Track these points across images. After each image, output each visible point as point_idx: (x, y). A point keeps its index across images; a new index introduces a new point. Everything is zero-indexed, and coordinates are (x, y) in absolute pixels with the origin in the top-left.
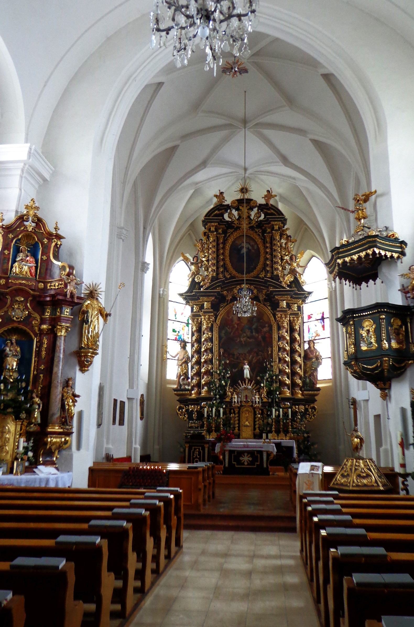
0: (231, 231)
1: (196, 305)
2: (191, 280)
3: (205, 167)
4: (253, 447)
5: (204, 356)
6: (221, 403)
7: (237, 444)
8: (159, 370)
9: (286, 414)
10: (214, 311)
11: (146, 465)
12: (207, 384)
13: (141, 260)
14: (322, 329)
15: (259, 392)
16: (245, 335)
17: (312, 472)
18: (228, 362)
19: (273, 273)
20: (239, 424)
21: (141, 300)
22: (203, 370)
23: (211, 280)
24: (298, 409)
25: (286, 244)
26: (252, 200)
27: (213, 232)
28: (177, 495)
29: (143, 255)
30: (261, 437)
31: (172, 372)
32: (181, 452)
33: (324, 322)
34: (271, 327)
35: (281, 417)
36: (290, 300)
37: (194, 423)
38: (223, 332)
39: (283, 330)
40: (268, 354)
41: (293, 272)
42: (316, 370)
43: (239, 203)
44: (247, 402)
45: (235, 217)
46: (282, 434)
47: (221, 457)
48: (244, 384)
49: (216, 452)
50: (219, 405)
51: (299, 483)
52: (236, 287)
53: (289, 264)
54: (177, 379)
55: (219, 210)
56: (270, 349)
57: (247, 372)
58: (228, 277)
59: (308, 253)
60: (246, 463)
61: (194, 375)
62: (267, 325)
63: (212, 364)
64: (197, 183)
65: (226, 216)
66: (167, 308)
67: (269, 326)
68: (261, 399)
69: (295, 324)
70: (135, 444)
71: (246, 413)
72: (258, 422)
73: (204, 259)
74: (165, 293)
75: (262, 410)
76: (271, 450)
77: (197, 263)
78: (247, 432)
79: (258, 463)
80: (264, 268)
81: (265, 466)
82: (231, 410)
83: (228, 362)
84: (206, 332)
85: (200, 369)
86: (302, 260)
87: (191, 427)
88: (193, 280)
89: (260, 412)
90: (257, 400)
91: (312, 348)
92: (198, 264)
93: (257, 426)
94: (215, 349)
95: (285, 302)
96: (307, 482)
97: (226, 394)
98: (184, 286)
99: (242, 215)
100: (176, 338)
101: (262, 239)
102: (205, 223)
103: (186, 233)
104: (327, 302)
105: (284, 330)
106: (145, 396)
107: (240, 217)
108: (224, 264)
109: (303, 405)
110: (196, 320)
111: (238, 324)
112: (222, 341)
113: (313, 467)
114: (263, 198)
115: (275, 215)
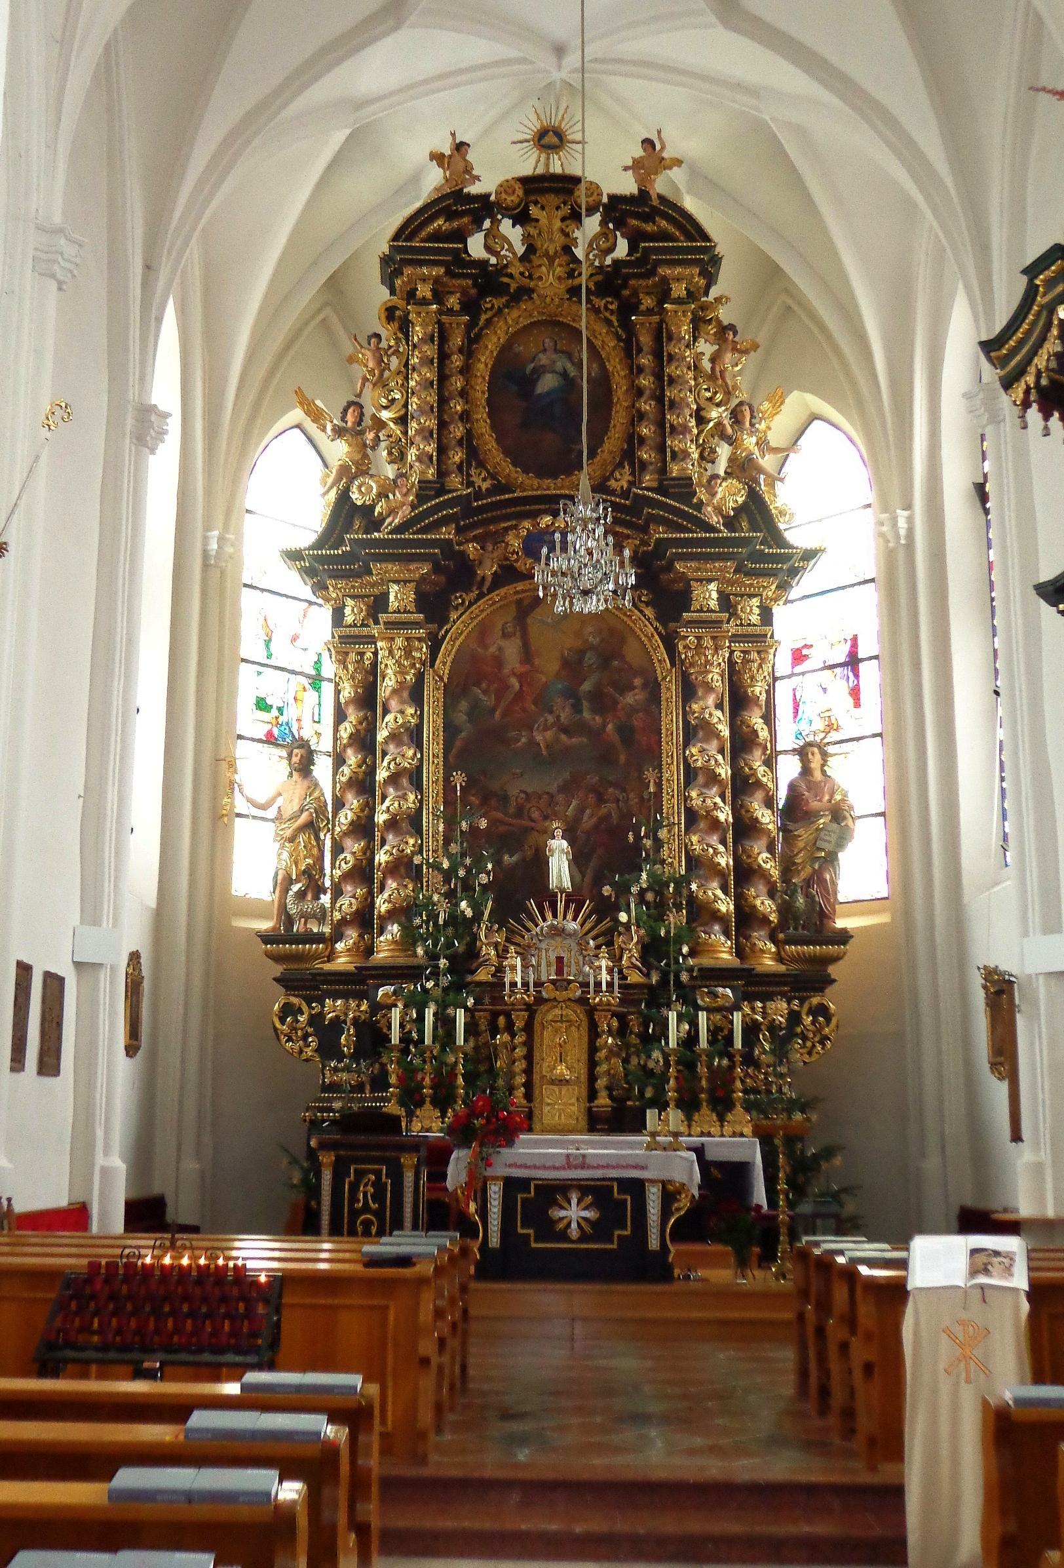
0: (498, 302)
1: (353, 597)
2: (333, 495)
3: (397, 27)
4: (607, 1167)
5: (387, 803)
6: (458, 986)
7: (538, 1153)
8: (204, 851)
9: (721, 1036)
10: (428, 620)
11: (173, 1246)
12: (403, 912)
13: (132, 394)
14: (851, 701)
15: (610, 944)
16: (551, 719)
17: (982, 1280)
18: (483, 824)
19: (663, 471)
20: (529, 1071)
21: (132, 581)
22: (382, 857)
23: (417, 496)
24: (764, 1014)
25: (713, 360)
26: (576, 180)
27: (424, 302)
28: (350, 1414)
29: (142, 379)
30: (637, 1125)
31: (256, 867)
32: (294, 1186)
33: (857, 676)
34: (654, 689)
35: (703, 1043)
36: (731, 583)
37: (347, 1069)
38: (464, 705)
39: (703, 698)
40: (642, 799)
41: (743, 468)
42: (831, 859)
43: (527, 192)
44: (561, 983)
45: (511, 248)
46: (706, 1115)
47: (472, 1207)
48: (549, 915)
49: (450, 1184)
50: (452, 996)
51: (916, 1333)
52: (515, 527)
53: (730, 441)
54: (276, 897)
55: (451, 215)
56: (650, 775)
57: (560, 869)
58: (485, 486)
59: (798, 402)
60: (574, 1232)
61: (347, 876)
62: (637, 682)
63: (418, 831)
64: (360, 104)
65: (476, 246)
66: (236, 615)
67: (645, 685)
68: (620, 972)
69: (752, 678)
70: (106, 1153)
71: (557, 1031)
72: (604, 1067)
73: (385, 415)
74: (229, 550)
75: (621, 1018)
76: (679, 1176)
77: (356, 426)
78: (561, 1104)
79: (627, 1232)
80: (628, 456)
81: (654, 1243)
82: (495, 1015)
83: (483, 824)
84: (394, 704)
85: (369, 852)
86: (778, 428)
87: (333, 1087)
88: (344, 497)
89: (615, 1024)
90: (605, 977)
91: (818, 775)
92: (362, 433)
93: (601, 1083)
94: (432, 774)
95: (713, 586)
96: (958, 1330)
97: (478, 955)
98: (308, 517)
99: (538, 244)
100: (270, 733)
101: (619, 339)
102: (391, 267)
103: (313, 317)
104: (870, 596)
105: (711, 700)
106: (145, 961)
107: (531, 249)
108: (469, 433)
109: (783, 995)
110: (353, 657)
111: (521, 677)
112: (458, 744)
113: (981, 1259)
114: (626, 169)
115: (677, 240)
